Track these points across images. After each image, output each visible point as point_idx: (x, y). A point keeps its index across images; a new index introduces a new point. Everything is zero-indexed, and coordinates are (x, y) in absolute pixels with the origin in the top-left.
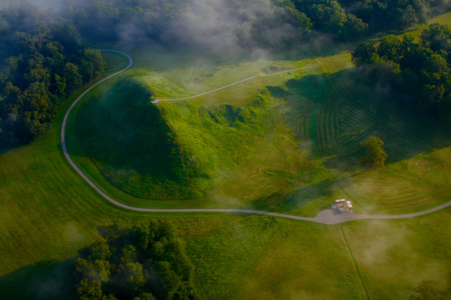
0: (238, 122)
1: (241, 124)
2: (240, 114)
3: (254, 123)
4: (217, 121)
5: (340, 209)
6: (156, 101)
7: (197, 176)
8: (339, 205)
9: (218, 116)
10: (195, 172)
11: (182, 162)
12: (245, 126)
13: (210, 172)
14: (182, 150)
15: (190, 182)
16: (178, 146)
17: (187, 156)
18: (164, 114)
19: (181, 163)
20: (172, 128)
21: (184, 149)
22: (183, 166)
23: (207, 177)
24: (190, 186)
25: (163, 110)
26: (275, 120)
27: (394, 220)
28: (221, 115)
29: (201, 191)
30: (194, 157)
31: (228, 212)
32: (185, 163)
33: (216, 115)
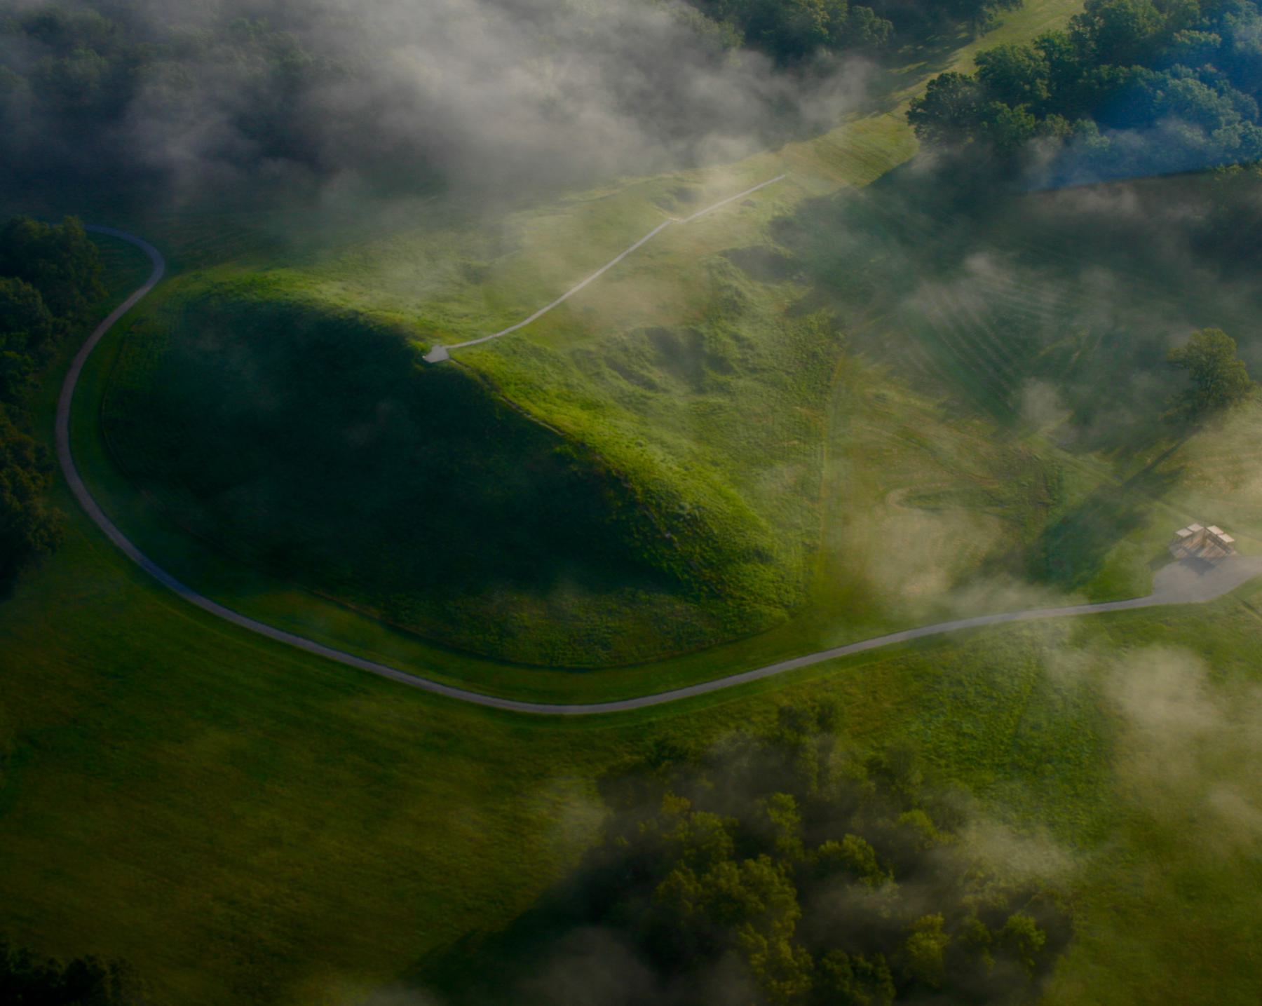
0: (712, 375)
1: (728, 378)
2: (707, 350)
3: (764, 370)
4: (650, 386)
5: (1201, 554)
6: (437, 354)
7: (730, 561)
8: (1188, 545)
9: (642, 367)
10: (718, 550)
11: (663, 529)
12: (741, 383)
13: (764, 542)
14: (639, 489)
15: (723, 582)
16: (618, 480)
17: (664, 504)
18: (497, 389)
19: (658, 531)
20: (558, 428)
21: (642, 485)
22: (670, 541)
23: (761, 556)
24: (731, 596)
25: (484, 377)
26: (818, 350)
27: (1101, 615)
28: (647, 364)
29: (769, 602)
30: (688, 507)
31: (902, 643)
32: (671, 529)
33: (636, 368)
